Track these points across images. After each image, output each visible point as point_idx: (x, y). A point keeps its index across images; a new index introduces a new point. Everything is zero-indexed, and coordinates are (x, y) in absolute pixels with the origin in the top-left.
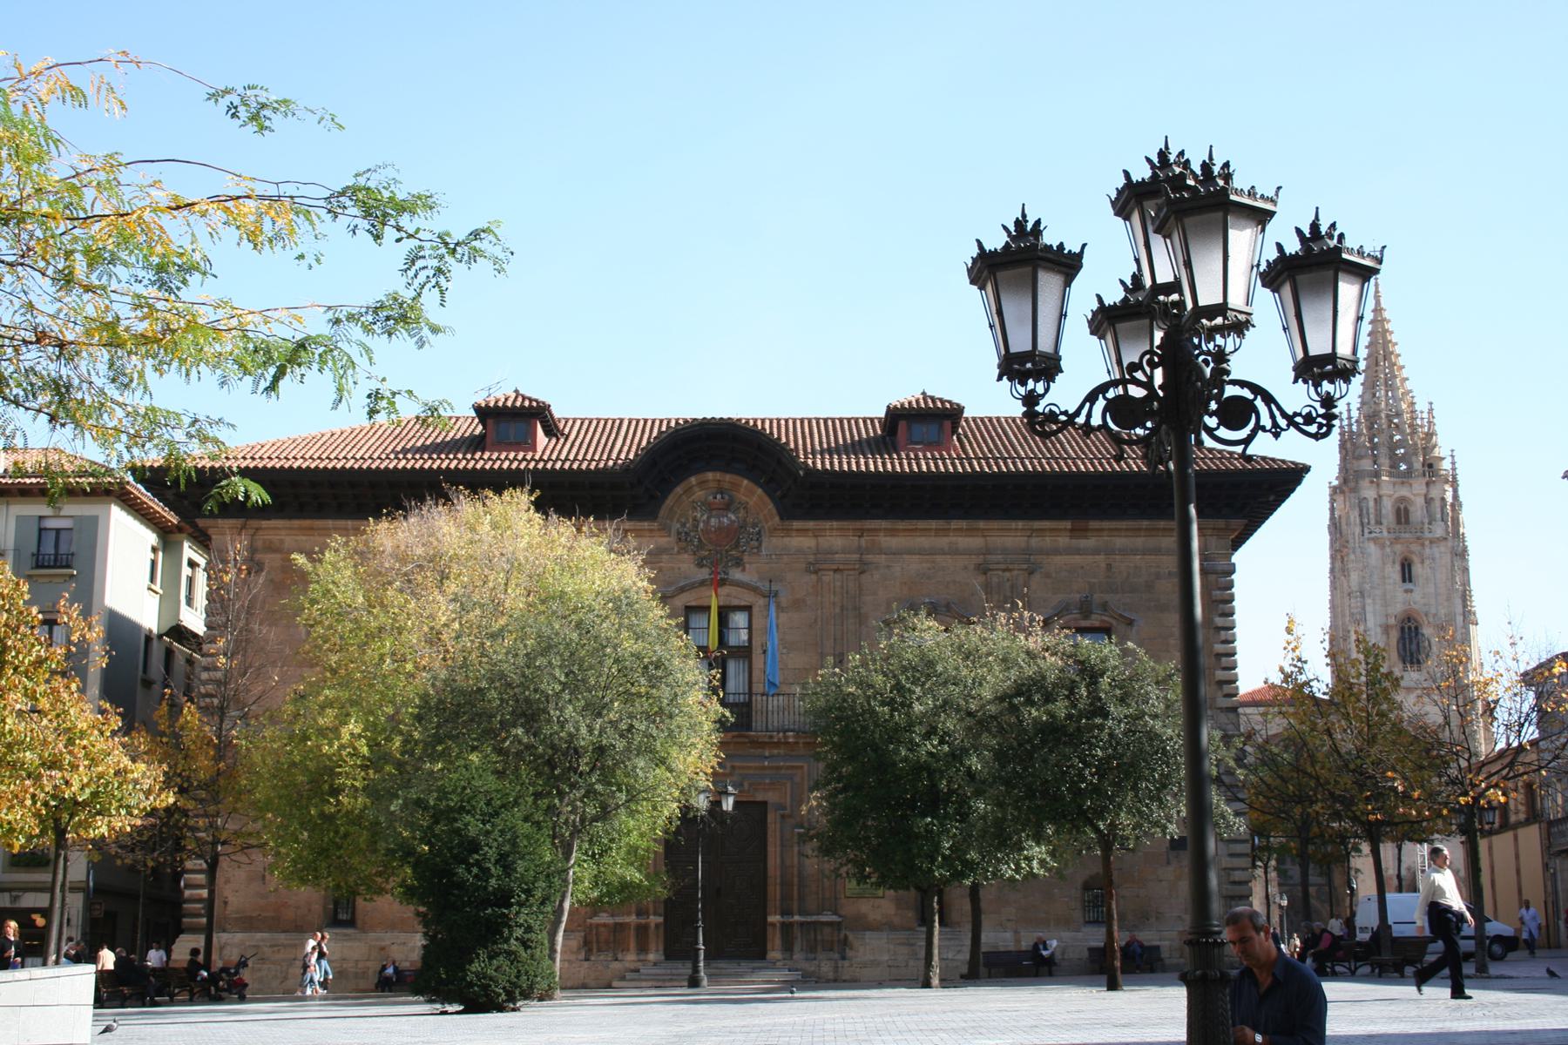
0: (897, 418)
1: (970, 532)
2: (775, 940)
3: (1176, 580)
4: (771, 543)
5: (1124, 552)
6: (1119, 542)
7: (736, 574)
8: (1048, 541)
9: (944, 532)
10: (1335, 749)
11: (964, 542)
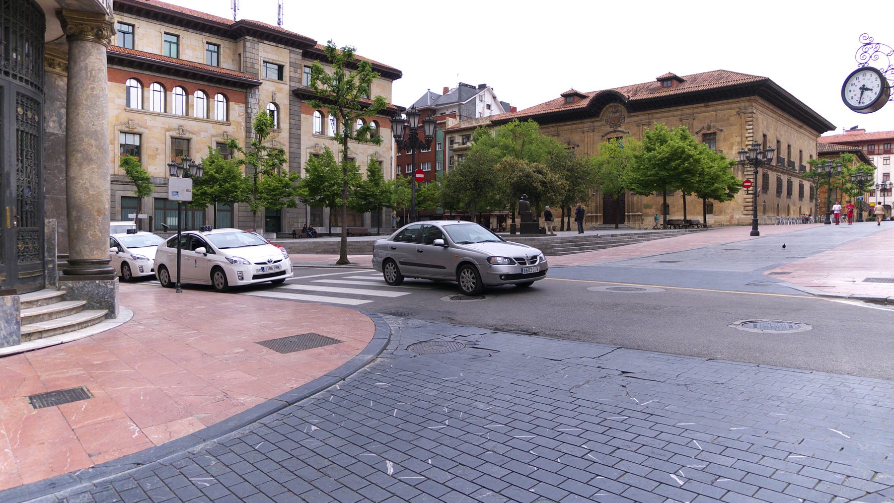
0: (661, 80)
1: (677, 110)
2: (626, 219)
3: (272, 22)
4: (627, 120)
5: (721, 110)
6: (720, 107)
7: (619, 129)
8: (699, 110)
9: (670, 111)
10: (323, 116)
11: (676, 113)
